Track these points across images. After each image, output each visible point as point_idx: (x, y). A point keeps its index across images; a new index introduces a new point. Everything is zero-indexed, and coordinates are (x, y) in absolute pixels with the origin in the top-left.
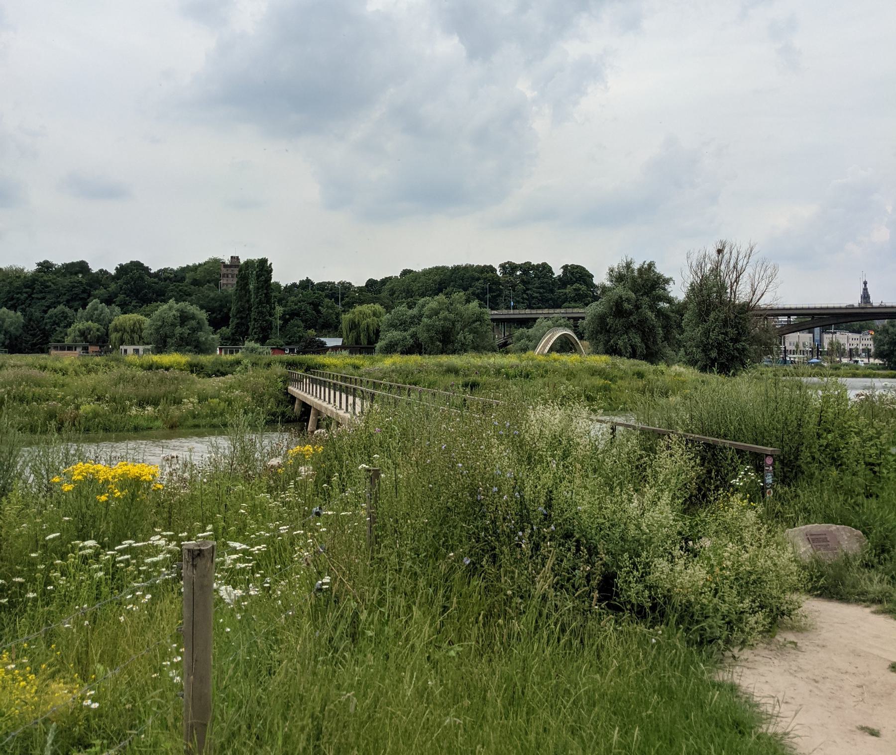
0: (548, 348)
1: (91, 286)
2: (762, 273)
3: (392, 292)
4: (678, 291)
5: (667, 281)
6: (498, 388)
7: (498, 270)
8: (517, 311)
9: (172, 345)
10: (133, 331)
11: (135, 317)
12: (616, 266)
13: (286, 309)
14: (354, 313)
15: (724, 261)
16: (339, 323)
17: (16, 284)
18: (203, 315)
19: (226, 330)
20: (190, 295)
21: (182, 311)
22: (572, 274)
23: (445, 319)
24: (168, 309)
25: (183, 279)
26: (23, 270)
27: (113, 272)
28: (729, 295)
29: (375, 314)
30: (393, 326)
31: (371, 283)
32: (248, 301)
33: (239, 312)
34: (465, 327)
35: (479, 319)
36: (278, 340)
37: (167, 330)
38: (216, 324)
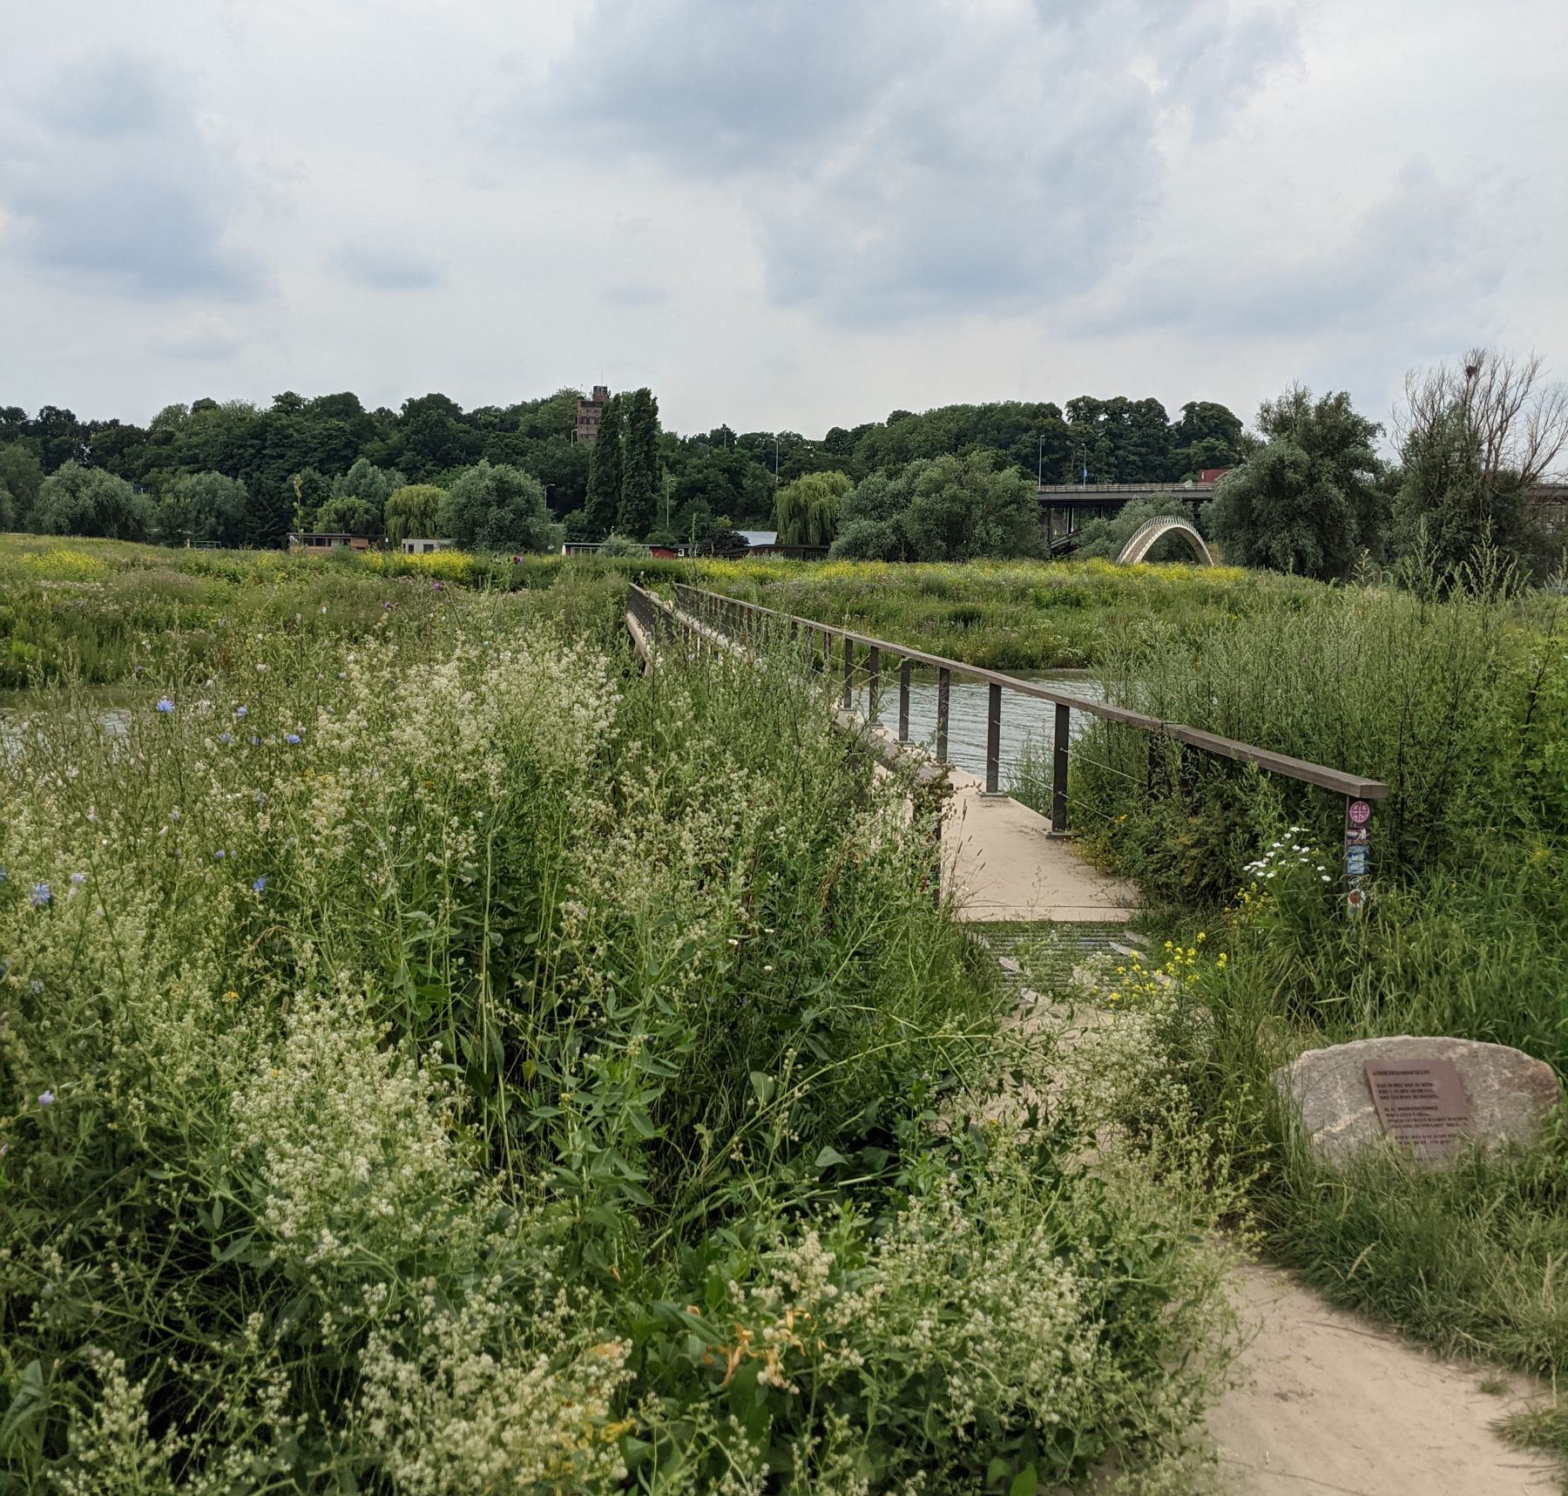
0: (1142, 554)
1: (359, 437)
2: (1553, 413)
3: (873, 451)
4: (1389, 450)
5: (1371, 430)
6: (1017, 623)
7: (1065, 411)
8: (1093, 488)
9: (484, 539)
10: (424, 514)
11: (426, 489)
12: (1274, 401)
13: (683, 480)
14: (797, 488)
15: (1479, 389)
16: (773, 504)
17: (237, 432)
18: (536, 488)
19: (580, 516)
20: (522, 454)
21: (501, 480)
22: (1202, 419)
23: (954, 498)
24: (478, 476)
25: (514, 426)
26: (251, 408)
27: (398, 412)
28: (1484, 455)
29: (834, 490)
30: (859, 510)
31: (836, 436)
32: (617, 465)
33: (600, 483)
34: (990, 513)
35: (1017, 499)
36: (665, 533)
37: (475, 511)
38: (561, 503)
